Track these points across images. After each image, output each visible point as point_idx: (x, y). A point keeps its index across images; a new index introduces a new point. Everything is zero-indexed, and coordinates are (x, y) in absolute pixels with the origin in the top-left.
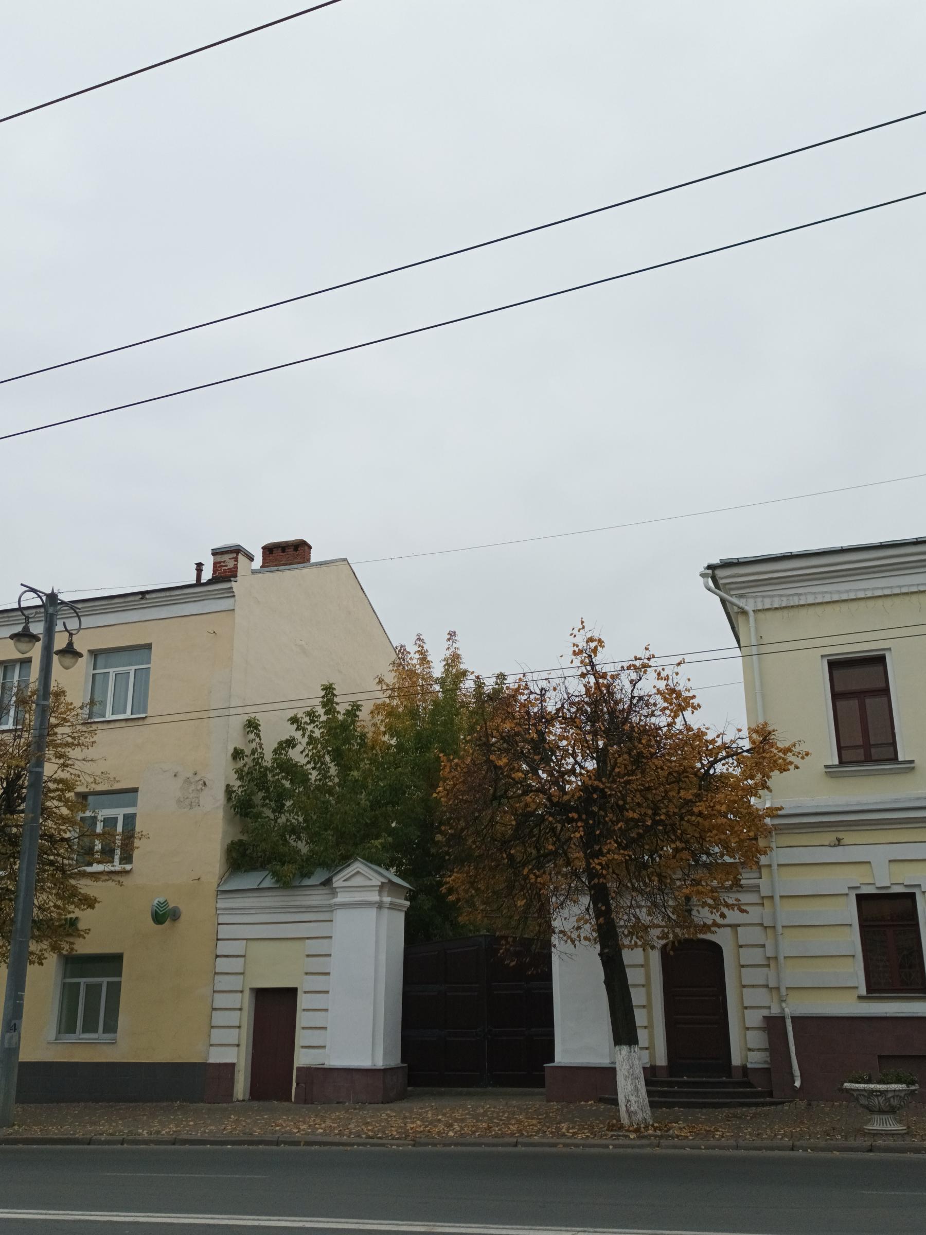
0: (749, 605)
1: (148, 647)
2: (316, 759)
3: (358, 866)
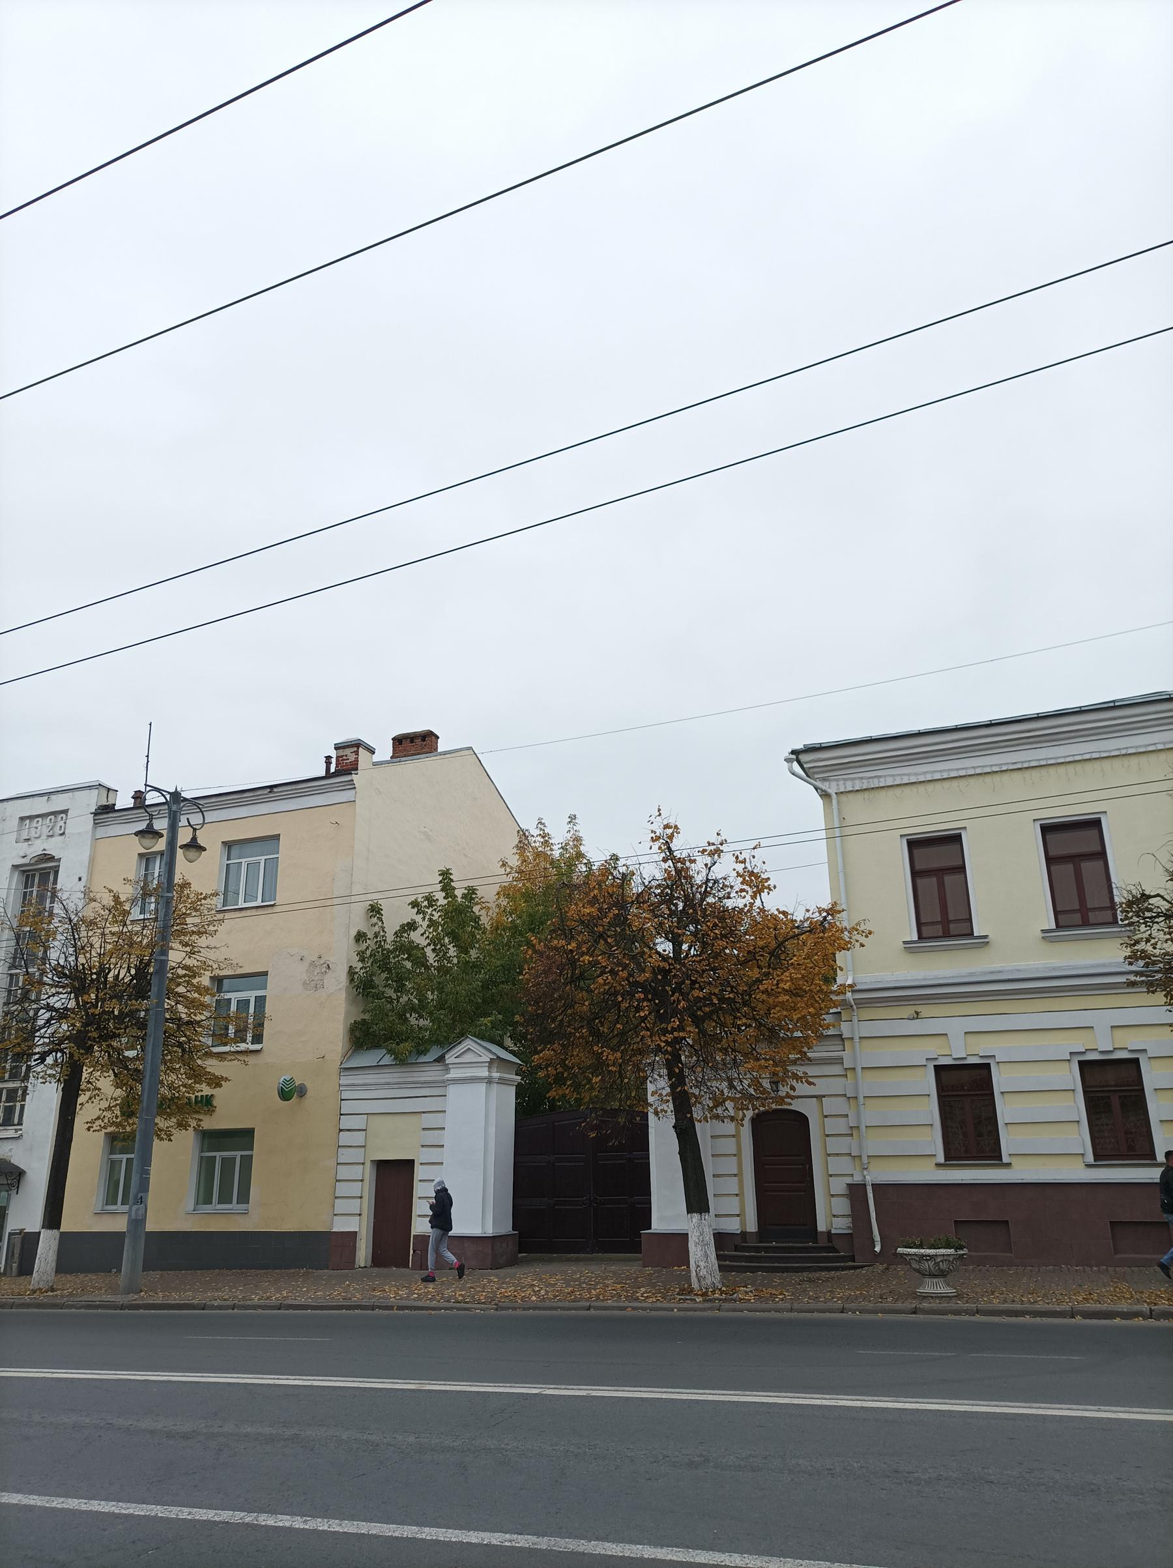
0: (832, 791)
1: (277, 837)
2: (435, 941)
3: (468, 1043)
